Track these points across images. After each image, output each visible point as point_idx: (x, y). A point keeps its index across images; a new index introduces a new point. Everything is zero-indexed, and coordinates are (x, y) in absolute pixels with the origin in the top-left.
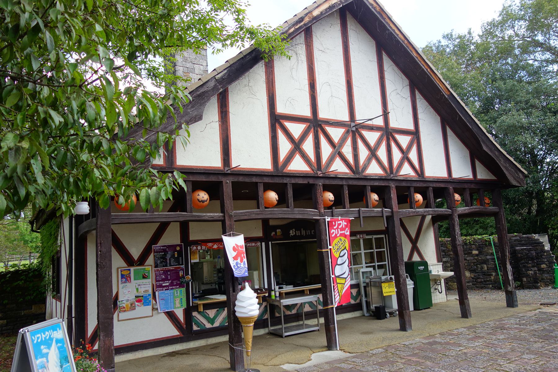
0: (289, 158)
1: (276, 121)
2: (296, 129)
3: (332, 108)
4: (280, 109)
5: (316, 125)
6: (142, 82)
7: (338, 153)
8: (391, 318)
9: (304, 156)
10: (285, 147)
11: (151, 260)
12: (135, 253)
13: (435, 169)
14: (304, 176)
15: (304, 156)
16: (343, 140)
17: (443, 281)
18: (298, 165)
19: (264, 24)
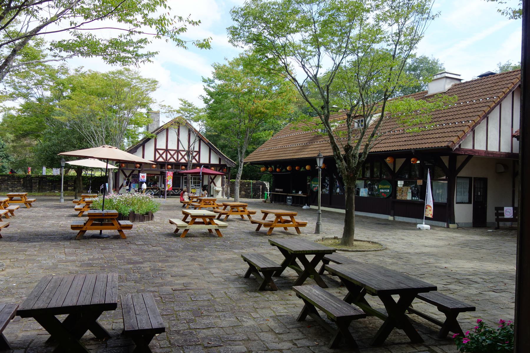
0: (159, 158)
1: (156, 150)
2: (172, 153)
3: (172, 146)
4: (157, 147)
5: (167, 150)
6: (203, 127)
7: (172, 156)
8: (475, 237)
9: (185, 159)
10: (158, 155)
11: (131, 177)
12: (127, 175)
13: (204, 160)
14: (162, 162)
15: (185, 159)
16: (174, 154)
17: (429, 212)
18: (161, 160)
19: (169, 106)
